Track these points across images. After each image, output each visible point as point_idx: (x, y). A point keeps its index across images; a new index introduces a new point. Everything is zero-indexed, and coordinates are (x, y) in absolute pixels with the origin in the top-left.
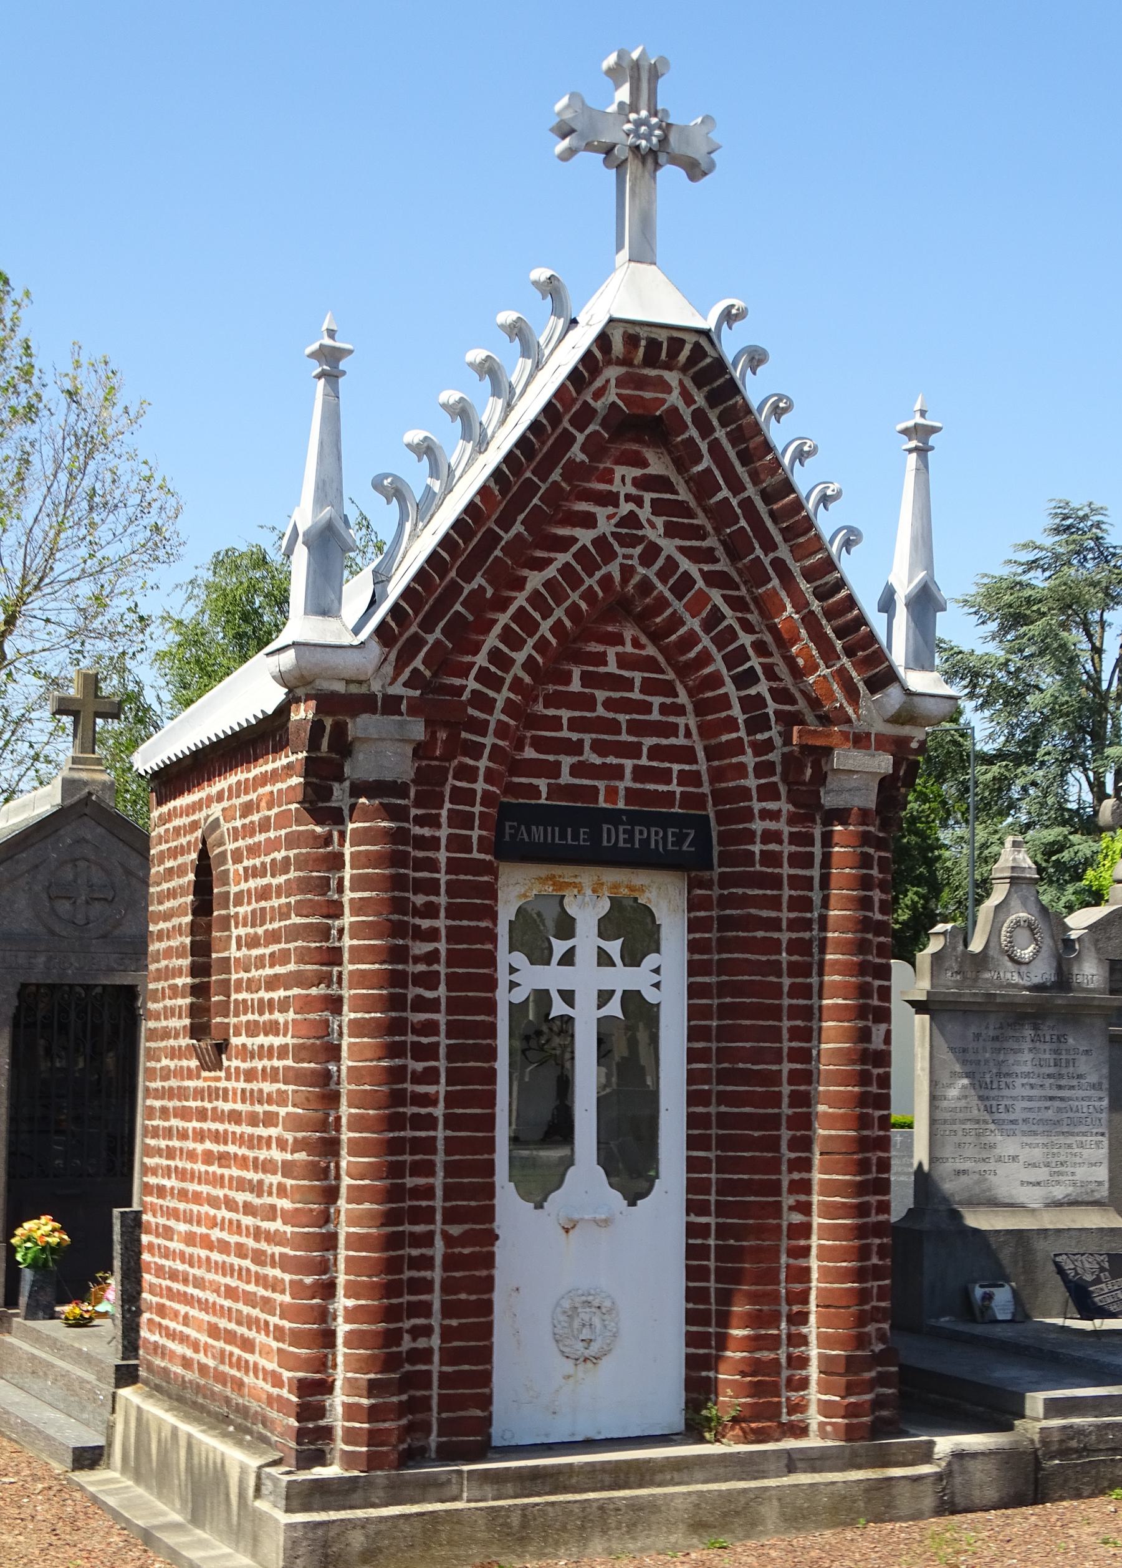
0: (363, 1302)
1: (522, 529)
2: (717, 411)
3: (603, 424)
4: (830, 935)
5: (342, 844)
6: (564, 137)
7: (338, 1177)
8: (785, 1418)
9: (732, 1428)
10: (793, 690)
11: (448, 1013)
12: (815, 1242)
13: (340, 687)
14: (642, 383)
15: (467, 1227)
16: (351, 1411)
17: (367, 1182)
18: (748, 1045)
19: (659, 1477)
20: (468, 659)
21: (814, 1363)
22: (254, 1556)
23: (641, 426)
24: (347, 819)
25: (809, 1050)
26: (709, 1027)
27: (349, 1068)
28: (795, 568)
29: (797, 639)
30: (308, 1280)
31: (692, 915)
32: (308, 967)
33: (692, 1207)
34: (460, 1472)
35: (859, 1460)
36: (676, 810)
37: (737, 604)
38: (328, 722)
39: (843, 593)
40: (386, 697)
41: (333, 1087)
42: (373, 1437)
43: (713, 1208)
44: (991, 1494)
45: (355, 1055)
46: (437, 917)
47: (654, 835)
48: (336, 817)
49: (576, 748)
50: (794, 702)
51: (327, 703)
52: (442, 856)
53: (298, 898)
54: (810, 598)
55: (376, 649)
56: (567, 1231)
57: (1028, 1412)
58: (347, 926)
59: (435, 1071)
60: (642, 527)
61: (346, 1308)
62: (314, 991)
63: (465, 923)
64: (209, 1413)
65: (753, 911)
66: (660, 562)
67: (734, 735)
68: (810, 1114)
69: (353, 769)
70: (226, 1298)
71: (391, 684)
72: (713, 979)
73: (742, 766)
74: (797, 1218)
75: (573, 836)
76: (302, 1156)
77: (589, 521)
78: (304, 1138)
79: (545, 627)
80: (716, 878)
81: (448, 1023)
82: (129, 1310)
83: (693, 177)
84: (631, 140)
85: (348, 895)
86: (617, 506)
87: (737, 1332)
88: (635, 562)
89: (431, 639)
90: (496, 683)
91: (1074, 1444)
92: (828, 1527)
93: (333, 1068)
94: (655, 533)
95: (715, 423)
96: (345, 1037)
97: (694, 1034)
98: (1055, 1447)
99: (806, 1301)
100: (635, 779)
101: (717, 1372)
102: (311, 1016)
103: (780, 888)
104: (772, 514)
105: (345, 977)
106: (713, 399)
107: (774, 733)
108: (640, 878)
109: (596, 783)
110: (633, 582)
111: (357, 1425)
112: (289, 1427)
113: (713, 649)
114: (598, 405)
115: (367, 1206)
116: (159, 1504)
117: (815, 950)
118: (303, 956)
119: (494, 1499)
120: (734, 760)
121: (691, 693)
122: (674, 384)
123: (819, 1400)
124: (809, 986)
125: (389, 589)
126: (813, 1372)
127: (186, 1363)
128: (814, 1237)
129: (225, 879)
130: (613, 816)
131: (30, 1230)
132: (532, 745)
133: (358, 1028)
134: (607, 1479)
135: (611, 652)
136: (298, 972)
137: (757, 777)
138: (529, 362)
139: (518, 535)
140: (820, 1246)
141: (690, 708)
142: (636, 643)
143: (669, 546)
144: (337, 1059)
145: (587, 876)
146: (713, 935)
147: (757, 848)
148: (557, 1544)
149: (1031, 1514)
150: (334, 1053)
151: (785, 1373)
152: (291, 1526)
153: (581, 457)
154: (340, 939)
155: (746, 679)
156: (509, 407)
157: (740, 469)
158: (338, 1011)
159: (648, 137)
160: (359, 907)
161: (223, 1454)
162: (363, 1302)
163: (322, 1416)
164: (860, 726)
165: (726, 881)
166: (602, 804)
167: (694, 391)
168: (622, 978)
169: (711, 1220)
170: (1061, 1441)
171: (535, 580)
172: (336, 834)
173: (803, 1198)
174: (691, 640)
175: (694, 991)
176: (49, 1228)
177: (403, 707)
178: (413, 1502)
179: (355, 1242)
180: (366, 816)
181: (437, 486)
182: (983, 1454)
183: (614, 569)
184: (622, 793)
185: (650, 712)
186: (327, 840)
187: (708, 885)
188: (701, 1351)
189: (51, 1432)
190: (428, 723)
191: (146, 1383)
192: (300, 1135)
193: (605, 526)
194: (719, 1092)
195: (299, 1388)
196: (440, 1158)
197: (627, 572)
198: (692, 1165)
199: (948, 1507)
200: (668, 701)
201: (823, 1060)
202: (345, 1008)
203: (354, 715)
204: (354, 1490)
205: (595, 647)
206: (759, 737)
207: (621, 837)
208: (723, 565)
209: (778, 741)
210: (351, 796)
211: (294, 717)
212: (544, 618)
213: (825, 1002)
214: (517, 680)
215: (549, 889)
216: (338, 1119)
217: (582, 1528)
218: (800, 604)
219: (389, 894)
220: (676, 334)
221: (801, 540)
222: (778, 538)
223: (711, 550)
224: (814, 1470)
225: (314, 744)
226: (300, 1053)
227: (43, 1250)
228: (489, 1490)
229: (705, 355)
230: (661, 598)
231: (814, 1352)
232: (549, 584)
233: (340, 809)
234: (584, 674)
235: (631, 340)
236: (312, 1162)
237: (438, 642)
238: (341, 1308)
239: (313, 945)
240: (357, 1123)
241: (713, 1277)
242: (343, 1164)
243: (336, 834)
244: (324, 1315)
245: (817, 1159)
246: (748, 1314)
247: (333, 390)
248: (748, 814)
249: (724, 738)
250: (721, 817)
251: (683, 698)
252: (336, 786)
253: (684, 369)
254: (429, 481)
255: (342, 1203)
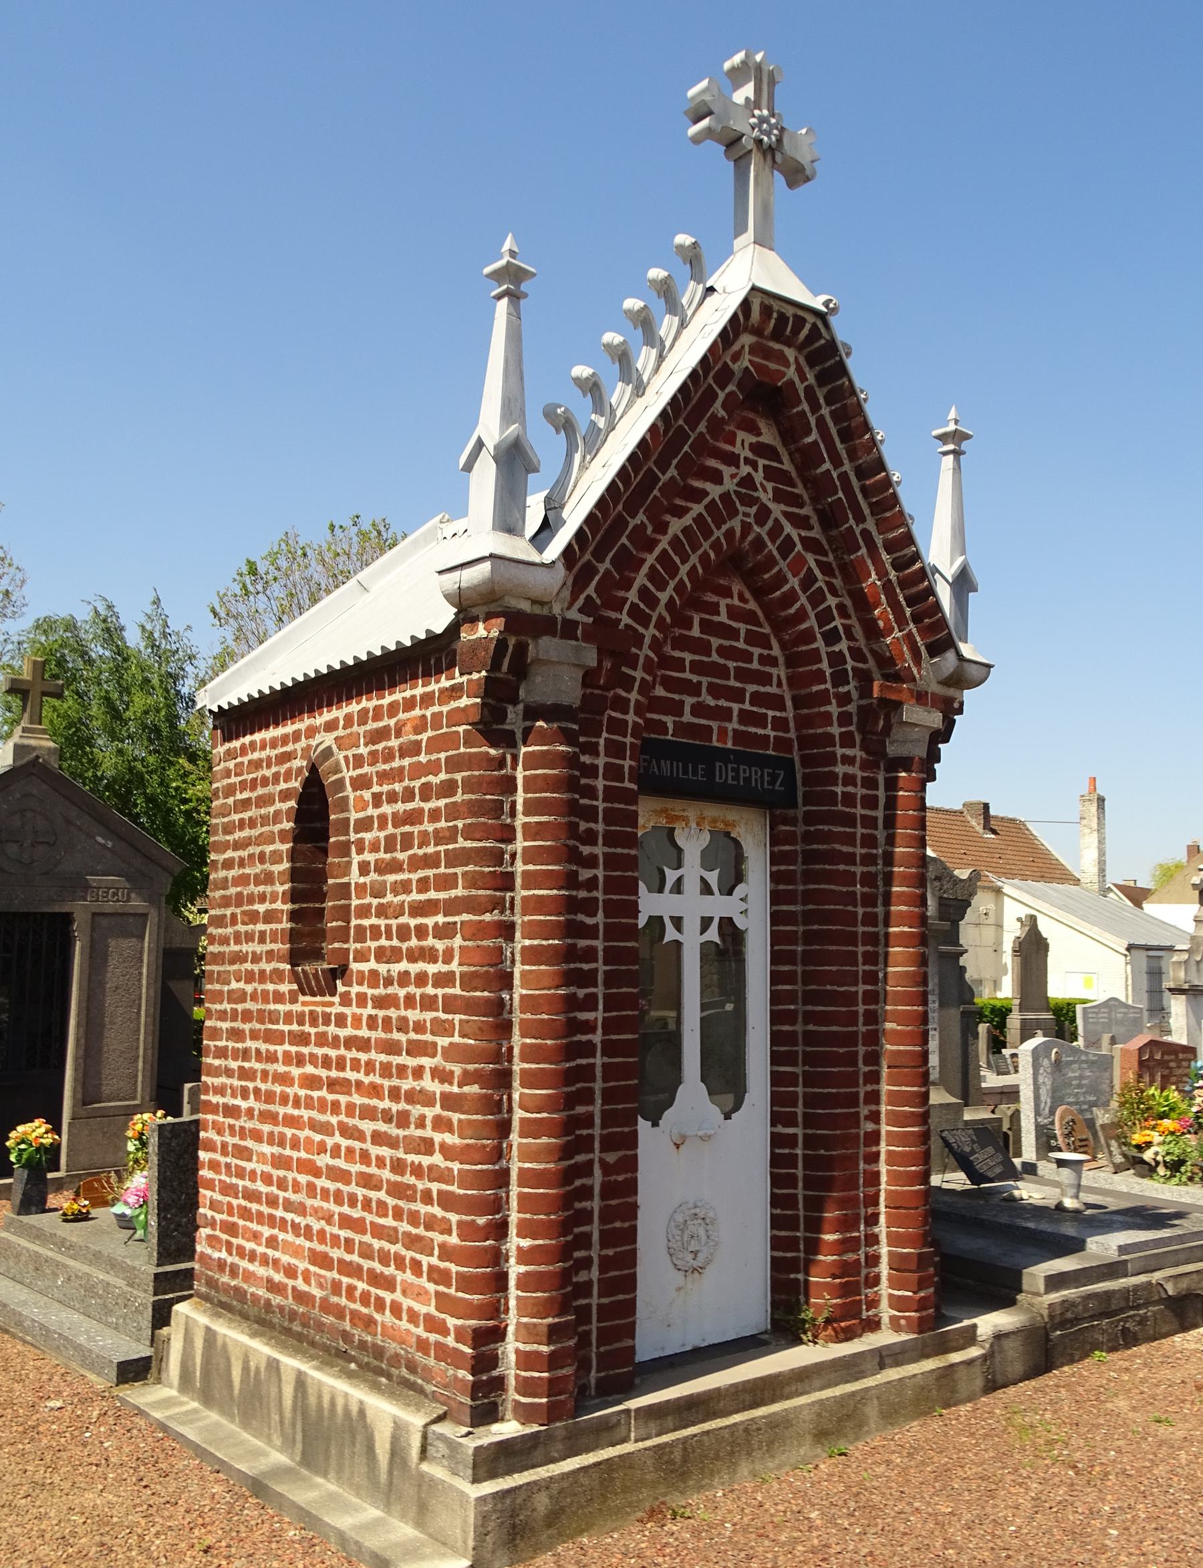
0: (541, 1242)
1: (675, 473)
2: (825, 390)
3: (739, 386)
4: (896, 869)
5: (514, 768)
6: (697, 120)
7: (510, 1110)
8: (864, 1315)
9: (825, 1329)
10: (865, 650)
11: (605, 940)
12: (883, 1148)
13: (525, 606)
14: (768, 354)
15: (621, 1153)
16: (526, 1361)
17: (545, 1115)
18: (834, 968)
19: (787, 1390)
20: (621, 594)
21: (884, 1260)
22: (420, 1524)
23: (766, 397)
24: (520, 742)
25: (876, 973)
26: (794, 952)
27: (522, 997)
28: (879, 540)
29: (878, 604)
30: (481, 1221)
31: (776, 849)
32: (481, 892)
33: (776, 1119)
34: (628, 1411)
35: (928, 1350)
36: (770, 752)
37: (826, 568)
38: (512, 641)
39: (918, 565)
40: (565, 620)
41: (506, 1016)
42: (553, 1387)
43: (800, 1120)
44: (1018, 1368)
45: (527, 982)
46: (595, 844)
47: (754, 773)
48: (507, 740)
49: (694, 690)
50: (865, 661)
51: (517, 622)
52: (600, 784)
53: (469, 821)
54: (889, 568)
55: (561, 569)
56: (678, 1146)
57: (1025, 1287)
58: (519, 851)
59: (594, 997)
60: (756, 490)
61: (519, 1248)
62: (487, 917)
63: (619, 850)
64: (313, 1344)
65: (837, 846)
66: (770, 523)
67: (823, 687)
68: (877, 1031)
69: (528, 692)
70: (340, 1228)
71: (568, 608)
72: (798, 908)
73: (828, 715)
74: (870, 1126)
75: (685, 770)
76: (474, 1089)
77: (717, 478)
78: (476, 1070)
79: (684, 570)
80: (800, 816)
81: (606, 949)
82: (165, 1218)
83: (791, 184)
84: (756, 133)
85: (521, 819)
86: (738, 467)
87: (829, 1237)
88: (751, 520)
89: (602, 568)
90: (644, 620)
91: (1069, 1315)
92: (914, 1419)
93: (506, 996)
94: (766, 497)
95: (822, 401)
96: (518, 964)
97: (776, 958)
98: (1057, 1320)
99: (877, 1204)
100: (740, 722)
101: (807, 1273)
102: (484, 943)
103: (855, 826)
104: (864, 489)
105: (518, 902)
106: (822, 379)
107: (851, 687)
108: (732, 814)
109: (711, 723)
110: (750, 538)
111: (536, 1374)
112: (463, 1380)
113: (809, 608)
114: (735, 367)
115: (544, 1140)
116: (246, 1436)
117: (880, 883)
118: (473, 881)
119: (658, 1435)
120: (822, 709)
121: (783, 646)
122: (792, 360)
123: (890, 1295)
124: (875, 915)
125: (565, 515)
126: (884, 1269)
127: (273, 1287)
128: (883, 1144)
129: (343, 805)
130: (723, 754)
131: (25, 1133)
132: (662, 684)
133: (531, 955)
134: (748, 1398)
135: (723, 603)
136: (464, 898)
137: (840, 726)
138: (676, 319)
139: (672, 478)
140: (889, 1153)
141: (781, 660)
142: (742, 598)
143: (777, 509)
144: (510, 987)
145: (692, 810)
146: (797, 868)
147: (839, 790)
148: (712, 1474)
149: (1048, 1380)
150: (506, 981)
151: (864, 1272)
152: (481, 1500)
153: (722, 413)
154: (512, 864)
155: (831, 637)
156: (661, 358)
157: (840, 446)
158: (510, 938)
159: (768, 134)
160: (532, 832)
161: (361, 1402)
162: (541, 1242)
163: (495, 1366)
164: (921, 685)
165: (810, 818)
166: (715, 744)
167: (807, 369)
168: (720, 906)
169: (798, 1131)
170: (1062, 1314)
171: (676, 526)
172: (509, 757)
173: (873, 1108)
174: (791, 597)
175: (776, 918)
176: (43, 1130)
177: (579, 632)
178: (588, 1450)
179: (527, 1178)
180: (543, 739)
181: (601, 422)
182: (1013, 1333)
183: (736, 524)
184: (730, 734)
185: (751, 662)
186: (501, 763)
187: (793, 821)
188: (789, 1255)
189: (82, 1340)
190: (600, 652)
191: (206, 1298)
192: (471, 1067)
193: (729, 485)
194: (805, 1012)
195: (473, 1339)
196: (598, 1086)
197: (746, 528)
198: (776, 1079)
199: (992, 1386)
200: (765, 652)
201: (890, 982)
202: (518, 935)
203: (536, 637)
204: (535, 1447)
205: (711, 598)
206: (841, 689)
207: (730, 774)
208: (816, 533)
209: (855, 695)
210: (525, 719)
211: (464, 635)
212: (683, 563)
213: (892, 930)
214: (661, 618)
215: (663, 822)
216: (511, 1049)
217: (732, 1453)
218: (882, 573)
219: (566, 819)
220: (800, 313)
221: (888, 514)
222: (867, 511)
223: (807, 517)
224: (898, 1364)
225: (495, 665)
226: (468, 981)
227: (38, 1150)
228: (653, 1426)
229: (820, 336)
230: (770, 556)
231: (884, 1250)
232: (686, 530)
233: (513, 733)
234: (702, 621)
235: (766, 310)
236: (485, 1096)
237: (607, 572)
238: (514, 1248)
239: (487, 869)
240: (529, 1054)
241: (800, 1184)
242: (516, 1096)
243: (509, 757)
244: (497, 1258)
245: (885, 1071)
246: (837, 1219)
247: (515, 313)
248: (831, 759)
249: (815, 688)
250: (805, 760)
251: (776, 651)
252: (510, 708)
253: (800, 348)
254: (593, 417)
255: (515, 1137)
